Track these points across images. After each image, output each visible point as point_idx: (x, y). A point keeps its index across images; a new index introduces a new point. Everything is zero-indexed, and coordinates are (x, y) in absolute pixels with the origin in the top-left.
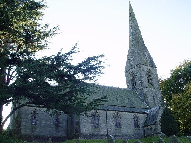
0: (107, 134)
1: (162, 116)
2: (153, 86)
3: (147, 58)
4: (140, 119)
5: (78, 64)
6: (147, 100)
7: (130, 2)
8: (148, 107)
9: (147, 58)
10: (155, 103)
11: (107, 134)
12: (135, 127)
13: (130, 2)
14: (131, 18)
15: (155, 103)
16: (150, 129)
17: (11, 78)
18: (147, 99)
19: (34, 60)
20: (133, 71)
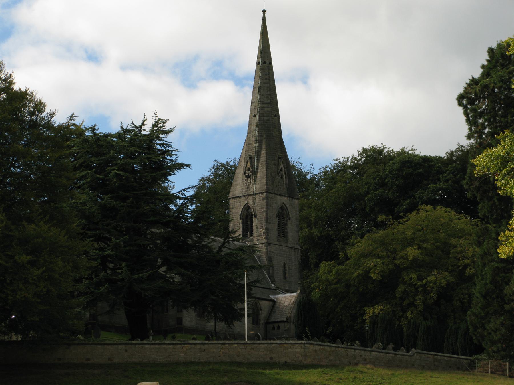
0: (215, 330)
1: (433, 352)
2: (287, 242)
3: (284, 176)
4: (261, 310)
5: (176, 172)
6: (271, 271)
7: (264, 11)
8: (273, 285)
9: (284, 176)
10: (285, 278)
11: (215, 330)
12: (253, 323)
13: (264, 11)
14: (267, 62)
15: (285, 278)
16: (276, 328)
17: (187, 190)
18: (273, 270)
19: (144, 133)
20: (251, 202)
